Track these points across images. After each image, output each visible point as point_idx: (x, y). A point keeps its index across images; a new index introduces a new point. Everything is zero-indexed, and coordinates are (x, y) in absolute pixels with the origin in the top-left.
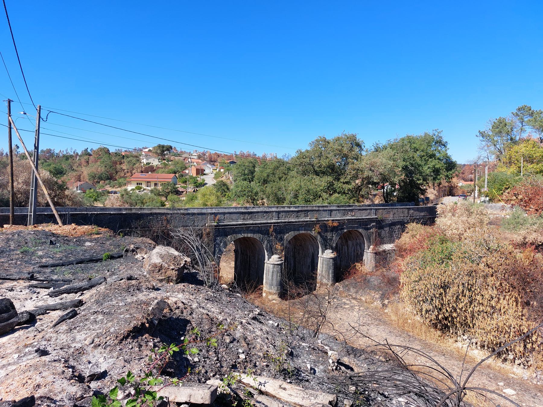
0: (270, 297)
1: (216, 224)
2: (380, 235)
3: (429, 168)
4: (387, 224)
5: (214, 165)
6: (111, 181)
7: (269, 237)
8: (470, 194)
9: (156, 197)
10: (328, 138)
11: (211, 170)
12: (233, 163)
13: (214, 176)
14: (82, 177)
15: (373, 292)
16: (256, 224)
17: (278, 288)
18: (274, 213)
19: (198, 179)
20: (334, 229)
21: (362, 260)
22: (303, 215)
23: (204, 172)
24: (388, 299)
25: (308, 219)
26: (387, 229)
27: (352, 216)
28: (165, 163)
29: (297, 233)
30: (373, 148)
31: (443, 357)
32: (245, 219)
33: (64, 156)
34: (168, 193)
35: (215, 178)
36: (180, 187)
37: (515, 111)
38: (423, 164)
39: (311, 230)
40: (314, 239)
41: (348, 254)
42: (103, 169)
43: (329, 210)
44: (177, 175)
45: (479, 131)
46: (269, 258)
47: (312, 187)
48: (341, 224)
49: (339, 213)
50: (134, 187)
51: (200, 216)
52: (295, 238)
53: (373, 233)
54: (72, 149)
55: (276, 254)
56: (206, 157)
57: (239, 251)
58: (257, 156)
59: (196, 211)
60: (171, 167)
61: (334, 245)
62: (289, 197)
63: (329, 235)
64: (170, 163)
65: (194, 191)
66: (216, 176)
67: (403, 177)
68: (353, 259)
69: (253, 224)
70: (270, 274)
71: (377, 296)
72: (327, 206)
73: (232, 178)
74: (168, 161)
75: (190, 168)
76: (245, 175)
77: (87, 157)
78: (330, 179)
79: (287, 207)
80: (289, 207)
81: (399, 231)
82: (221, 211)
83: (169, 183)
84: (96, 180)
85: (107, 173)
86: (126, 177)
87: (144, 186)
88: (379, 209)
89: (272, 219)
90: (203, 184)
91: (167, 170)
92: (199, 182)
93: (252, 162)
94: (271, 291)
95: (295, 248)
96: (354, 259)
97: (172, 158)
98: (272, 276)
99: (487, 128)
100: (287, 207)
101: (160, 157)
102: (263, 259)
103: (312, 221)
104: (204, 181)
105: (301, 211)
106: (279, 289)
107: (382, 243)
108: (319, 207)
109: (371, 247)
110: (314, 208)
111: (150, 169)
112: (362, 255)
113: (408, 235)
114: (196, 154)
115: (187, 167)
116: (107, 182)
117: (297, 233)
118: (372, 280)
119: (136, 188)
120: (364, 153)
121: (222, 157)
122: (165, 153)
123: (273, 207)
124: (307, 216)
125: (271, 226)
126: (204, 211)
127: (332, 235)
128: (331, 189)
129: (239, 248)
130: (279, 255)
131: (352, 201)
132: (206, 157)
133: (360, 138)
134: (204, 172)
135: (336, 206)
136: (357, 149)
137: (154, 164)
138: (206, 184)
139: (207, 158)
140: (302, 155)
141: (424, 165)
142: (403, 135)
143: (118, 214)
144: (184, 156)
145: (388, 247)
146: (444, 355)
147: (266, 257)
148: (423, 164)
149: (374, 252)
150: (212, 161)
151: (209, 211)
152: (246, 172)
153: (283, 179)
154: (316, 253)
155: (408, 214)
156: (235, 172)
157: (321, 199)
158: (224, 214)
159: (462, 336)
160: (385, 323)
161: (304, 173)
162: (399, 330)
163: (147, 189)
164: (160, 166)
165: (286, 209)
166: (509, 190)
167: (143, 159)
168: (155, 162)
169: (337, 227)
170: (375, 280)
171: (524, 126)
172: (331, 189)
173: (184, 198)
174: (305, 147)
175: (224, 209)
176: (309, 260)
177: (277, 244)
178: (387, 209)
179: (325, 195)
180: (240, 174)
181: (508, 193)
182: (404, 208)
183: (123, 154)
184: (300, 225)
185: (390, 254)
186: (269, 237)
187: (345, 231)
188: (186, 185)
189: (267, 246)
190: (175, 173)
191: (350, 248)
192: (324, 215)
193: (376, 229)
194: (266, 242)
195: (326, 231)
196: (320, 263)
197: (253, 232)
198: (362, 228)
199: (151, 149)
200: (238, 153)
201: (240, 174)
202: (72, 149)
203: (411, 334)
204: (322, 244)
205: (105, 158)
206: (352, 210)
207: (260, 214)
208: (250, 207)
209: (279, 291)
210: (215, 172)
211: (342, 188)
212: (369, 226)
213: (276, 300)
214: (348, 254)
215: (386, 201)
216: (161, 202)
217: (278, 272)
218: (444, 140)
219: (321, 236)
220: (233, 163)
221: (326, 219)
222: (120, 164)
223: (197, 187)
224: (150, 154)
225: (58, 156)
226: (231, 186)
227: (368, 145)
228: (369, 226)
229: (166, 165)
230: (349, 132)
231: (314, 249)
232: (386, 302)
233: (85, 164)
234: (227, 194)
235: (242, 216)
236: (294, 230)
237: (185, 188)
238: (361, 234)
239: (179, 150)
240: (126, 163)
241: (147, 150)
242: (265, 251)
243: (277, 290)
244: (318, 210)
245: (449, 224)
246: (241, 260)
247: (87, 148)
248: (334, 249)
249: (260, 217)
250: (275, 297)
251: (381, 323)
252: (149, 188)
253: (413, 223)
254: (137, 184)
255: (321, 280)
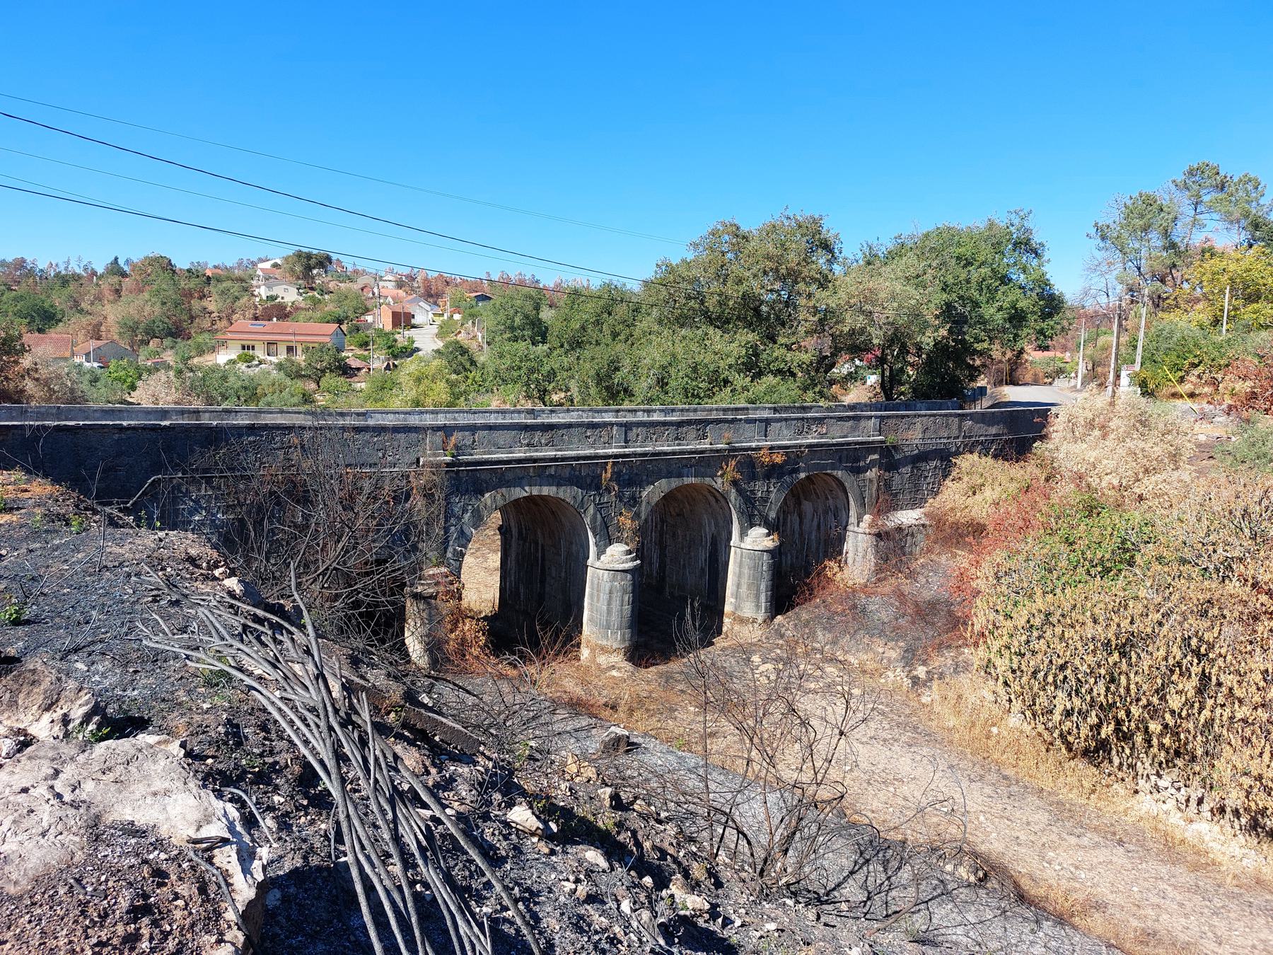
0: (603, 660)
1: (448, 459)
2: (888, 485)
3: (1000, 309)
4: (906, 457)
5: (435, 303)
6: (179, 340)
7: (601, 495)
8: (1050, 380)
9: (288, 382)
10: (744, 228)
11: (431, 316)
12: (484, 298)
13: (436, 331)
14: (103, 328)
15: (882, 643)
16: (563, 459)
17: (623, 635)
18: (615, 428)
19: (397, 336)
20: (773, 472)
21: (840, 553)
22: (692, 434)
23: (413, 321)
24: (924, 663)
25: (705, 445)
26: (907, 470)
27: (822, 435)
28: (314, 296)
29: (675, 483)
30: (860, 255)
31: (1121, 850)
32: (533, 445)
33: (58, 275)
34: (323, 371)
35: (440, 335)
36: (351, 356)
37: (1180, 178)
38: (985, 300)
39: (713, 476)
40: (721, 498)
41: (801, 534)
42: (158, 309)
43: (761, 420)
44: (344, 327)
45: (1096, 225)
46: (601, 553)
47: (708, 358)
48: (794, 457)
49: (787, 427)
50: (234, 357)
51: (401, 436)
52: (669, 497)
53: (871, 481)
54: (80, 260)
55: (619, 540)
56: (416, 285)
57: (515, 531)
58: (541, 286)
59: (389, 421)
60: (330, 307)
61: (773, 515)
62: (642, 386)
63: (759, 488)
64: (327, 297)
65: (388, 368)
66: (443, 332)
67: (943, 332)
68: (813, 549)
69: (555, 459)
70: (604, 597)
71: (893, 654)
72: (747, 409)
73: (483, 338)
74: (322, 292)
75: (376, 311)
76: (512, 329)
77: (116, 279)
78: (752, 337)
79: (644, 411)
80: (648, 411)
81: (935, 475)
82: (463, 420)
83: (323, 345)
84: (140, 337)
85: (167, 320)
86: (217, 331)
87: (260, 353)
88: (888, 417)
89: (608, 444)
90: (409, 351)
91: (318, 314)
92: (399, 345)
93: (531, 297)
94: (604, 643)
95: (662, 521)
96: (817, 549)
97: (331, 285)
98: (609, 604)
99: (1112, 217)
100: (644, 411)
101: (300, 282)
102: (581, 555)
103: (718, 451)
104: (413, 342)
105: (689, 422)
106: (628, 636)
107: (895, 507)
108: (725, 410)
109: (867, 518)
110: (714, 416)
111: (280, 312)
112: (841, 540)
113: (957, 485)
114: (391, 278)
115: (370, 307)
116: (168, 342)
117: (675, 483)
118: (872, 607)
119: (239, 357)
120: (837, 268)
121: (456, 286)
122: (315, 272)
123: (606, 411)
124: (705, 437)
125: (606, 463)
126: (414, 421)
127: (769, 487)
128: (752, 366)
129: (513, 524)
130: (627, 544)
131: (810, 394)
132: (416, 285)
133: (830, 228)
134: (413, 321)
135: (770, 409)
136: (821, 260)
137: (285, 300)
138: (418, 350)
139: (419, 287)
140: (669, 279)
141: (987, 302)
142: (927, 226)
143: (145, 428)
144: (361, 281)
145: (907, 517)
146: (1121, 842)
147: (593, 549)
148: (983, 299)
149: (874, 530)
150: (431, 295)
151: (429, 420)
152: (518, 320)
153: (622, 337)
154: (724, 535)
155: (960, 431)
156: (489, 321)
157: (729, 389)
158: (473, 429)
159: (1153, 778)
160: (930, 738)
161: (682, 321)
162: (975, 759)
163: (268, 363)
164: (303, 305)
165: (642, 417)
166: (1201, 368)
167: (259, 287)
168: (289, 295)
169: (781, 466)
170: (880, 609)
171: (1202, 213)
172: (752, 366)
173: (363, 385)
174: (679, 252)
175: (470, 416)
176: (703, 555)
177: (621, 514)
178: (908, 416)
179: (740, 380)
180: (503, 327)
181: (1199, 377)
182: (951, 415)
183: (209, 273)
184: (684, 461)
185: (913, 535)
186: (601, 495)
187: (802, 475)
188: (366, 353)
189: (594, 519)
190: (340, 322)
191: (807, 521)
192: (748, 434)
193: (880, 469)
194: (591, 510)
195: (753, 477)
196: (735, 562)
197: (558, 481)
198: (846, 468)
199: (279, 262)
200: (495, 277)
201: (503, 327)
202: (80, 260)
203: (1010, 772)
204: (741, 513)
205: (163, 282)
206: (820, 421)
207: (574, 431)
208: (543, 411)
209: (627, 644)
210: (438, 320)
211: (783, 361)
212: (862, 464)
213: (619, 669)
214: (801, 534)
215: (889, 397)
216: (304, 395)
217: (625, 592)
218: (1036, 239)
219: (740, 492)
220: (484, 298)
221: (754, 445)
222: (201, 298)
223: (395, 357)
224: (278, 273)
225: (44, 276)
226: (479, 356)
227: (850, 249)
228: (862, 464)
229: (316, 302)
230: (803, 209)
231: (717, 525)
232: (921, 671)
233: (111, 298)
234: (471, 376)
235: (524, 437)
236: (669, 475)
237: (365, 359)
238: (841, 484)
239: (349, 264)
240: (215, 296)
241: (267, 265)
242: (590, 534)
243: (623, 640)
244: (733, 421)
245: (1092, 460)
246: (518, 554)
247: (116, 259)
248: (772, 528)
249: (576, 440)
250: (616, 659)
251: (921, 740)
252: (274, 359)
253: (971, 453)
254: (243, 348)
255: (737, 607)
